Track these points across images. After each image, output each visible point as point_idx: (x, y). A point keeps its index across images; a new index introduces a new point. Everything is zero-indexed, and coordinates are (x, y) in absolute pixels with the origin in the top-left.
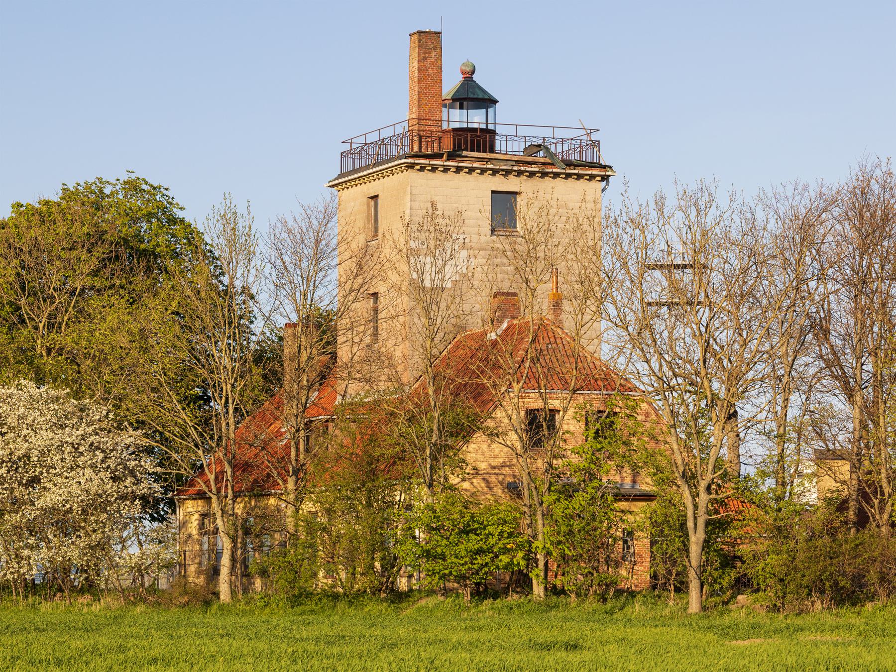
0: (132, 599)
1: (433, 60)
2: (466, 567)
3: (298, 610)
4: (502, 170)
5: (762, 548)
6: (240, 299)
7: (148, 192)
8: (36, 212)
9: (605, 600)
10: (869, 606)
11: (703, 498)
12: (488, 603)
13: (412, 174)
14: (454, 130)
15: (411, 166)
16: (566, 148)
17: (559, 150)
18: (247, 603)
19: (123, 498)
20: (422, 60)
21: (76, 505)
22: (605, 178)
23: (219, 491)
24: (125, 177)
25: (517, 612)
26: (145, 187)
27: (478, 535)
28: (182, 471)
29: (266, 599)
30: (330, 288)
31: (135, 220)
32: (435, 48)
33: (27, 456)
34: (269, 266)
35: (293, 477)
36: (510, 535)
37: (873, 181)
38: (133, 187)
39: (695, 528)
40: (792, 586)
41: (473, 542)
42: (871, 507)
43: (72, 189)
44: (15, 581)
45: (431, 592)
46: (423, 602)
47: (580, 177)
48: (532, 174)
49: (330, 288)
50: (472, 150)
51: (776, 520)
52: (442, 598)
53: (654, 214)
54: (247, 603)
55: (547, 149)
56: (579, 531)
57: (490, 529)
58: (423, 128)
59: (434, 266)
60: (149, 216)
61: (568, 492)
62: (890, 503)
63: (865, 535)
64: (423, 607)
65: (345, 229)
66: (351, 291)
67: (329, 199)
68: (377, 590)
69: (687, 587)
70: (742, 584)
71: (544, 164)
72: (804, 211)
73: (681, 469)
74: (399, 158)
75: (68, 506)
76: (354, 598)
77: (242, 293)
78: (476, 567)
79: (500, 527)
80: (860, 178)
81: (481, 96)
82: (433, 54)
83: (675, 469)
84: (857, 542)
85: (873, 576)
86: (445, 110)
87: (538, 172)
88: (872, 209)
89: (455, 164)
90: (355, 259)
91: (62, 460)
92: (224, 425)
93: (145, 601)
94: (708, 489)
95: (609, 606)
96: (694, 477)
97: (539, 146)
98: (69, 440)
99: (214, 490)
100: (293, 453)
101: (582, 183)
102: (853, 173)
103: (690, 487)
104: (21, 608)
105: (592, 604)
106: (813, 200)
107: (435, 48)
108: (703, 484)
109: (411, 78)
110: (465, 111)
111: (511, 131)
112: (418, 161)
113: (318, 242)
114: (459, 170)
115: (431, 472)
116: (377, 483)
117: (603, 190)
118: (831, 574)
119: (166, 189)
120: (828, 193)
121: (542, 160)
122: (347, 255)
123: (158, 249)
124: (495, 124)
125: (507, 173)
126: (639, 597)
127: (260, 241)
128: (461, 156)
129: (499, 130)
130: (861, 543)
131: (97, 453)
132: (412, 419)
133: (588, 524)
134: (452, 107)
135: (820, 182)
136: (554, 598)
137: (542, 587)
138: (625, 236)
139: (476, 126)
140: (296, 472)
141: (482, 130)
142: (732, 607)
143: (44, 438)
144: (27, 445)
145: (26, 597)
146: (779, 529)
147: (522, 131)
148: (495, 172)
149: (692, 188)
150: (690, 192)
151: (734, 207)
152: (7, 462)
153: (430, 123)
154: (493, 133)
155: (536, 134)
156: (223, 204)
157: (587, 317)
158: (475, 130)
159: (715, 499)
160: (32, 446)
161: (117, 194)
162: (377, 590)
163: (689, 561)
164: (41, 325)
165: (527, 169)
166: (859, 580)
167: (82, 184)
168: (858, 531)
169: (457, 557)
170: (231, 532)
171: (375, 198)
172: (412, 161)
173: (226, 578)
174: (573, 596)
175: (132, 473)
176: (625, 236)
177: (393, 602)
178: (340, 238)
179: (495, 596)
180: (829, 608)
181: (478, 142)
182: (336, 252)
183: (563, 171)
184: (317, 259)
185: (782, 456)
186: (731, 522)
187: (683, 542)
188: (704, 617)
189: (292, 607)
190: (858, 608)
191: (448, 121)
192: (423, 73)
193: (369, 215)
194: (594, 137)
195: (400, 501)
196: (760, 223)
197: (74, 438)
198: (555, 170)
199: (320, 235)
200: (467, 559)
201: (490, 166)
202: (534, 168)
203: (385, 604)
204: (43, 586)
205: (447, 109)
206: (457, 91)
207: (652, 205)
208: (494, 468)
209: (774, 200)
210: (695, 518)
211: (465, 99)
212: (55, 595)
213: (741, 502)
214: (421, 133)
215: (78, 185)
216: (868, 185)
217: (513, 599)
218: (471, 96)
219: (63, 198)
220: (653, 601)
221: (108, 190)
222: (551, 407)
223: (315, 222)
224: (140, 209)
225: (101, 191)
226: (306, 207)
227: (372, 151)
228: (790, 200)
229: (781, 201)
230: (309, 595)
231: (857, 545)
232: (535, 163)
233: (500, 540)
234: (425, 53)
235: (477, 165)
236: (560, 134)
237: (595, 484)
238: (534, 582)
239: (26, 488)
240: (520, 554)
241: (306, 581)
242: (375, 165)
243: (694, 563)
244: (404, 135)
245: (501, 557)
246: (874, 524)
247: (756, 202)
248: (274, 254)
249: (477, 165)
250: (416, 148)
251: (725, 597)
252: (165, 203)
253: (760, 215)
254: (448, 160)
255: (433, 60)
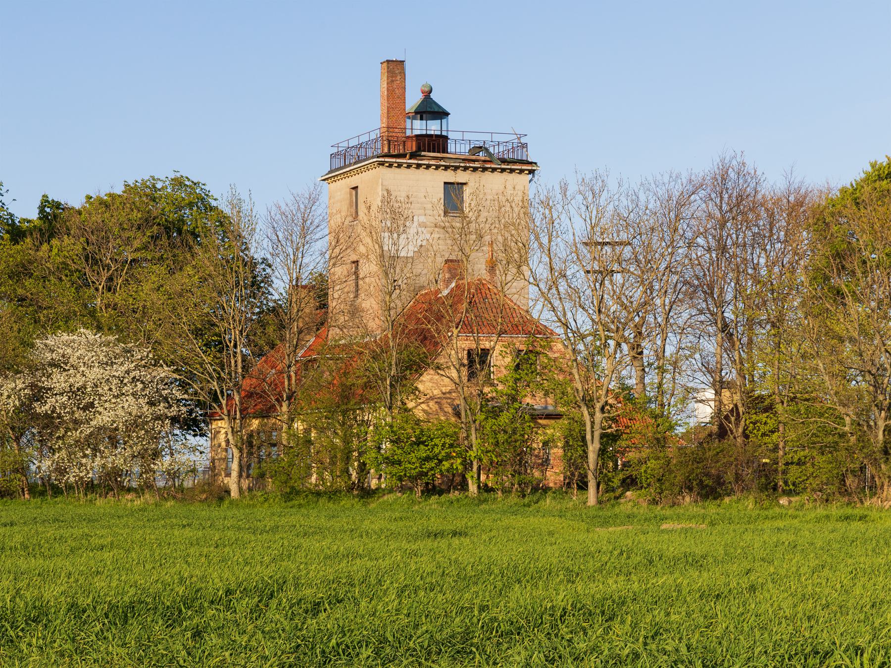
0: (166, 496)
1: (398, 82)
2: (417, 470)
3: (290, 504)
4: (452, 166)
5: (644, 455)
6: (260, 267)
7: (190, 187)
8: (102, 202)
9: (524, 496)
10: (727, 500)
11: (598, 416)
12: (434, 498)
13: (382, 170)
14: (417, 136)
15: (382, 164)
16: (501, 150)
17: (496, 151)
18: (251, 499)
19: (158, 418)
20: (390, 82)
21: (121, 424)
22: (531, 172)
23: (229, 411)
24: (172, 175)
25: (456, 506)
26: (187, 183)
27: (427, 446)
28: (201, 398)
29: (266, 496)
30: (314, 257)
31: (181, 208)
32: (400, 73)
33: (84, 387)
34: (267, 240)
35: (287, 402)
36: (451, 446)
37: (731, 170)
38: (178, 183)
39: (592, 440)
40: (667, 484)
41: (422, 452)
42: (729, 423)
43: (132, 185)
44: (76, 482)
45: (391, 491)
46: (386, 498)
47: (512, 171)
48: (475, 169)
49: (314, 257)
50: (429, 151)
51: (655, 433)
52: (399, 495)
53: (559, 197)
54: (251, 499)
55: (487, 150)
56: (503, 443)
57: (437, 441)
58: (391, 134)
59: (391, 240)
60: (191, 205)
61: (495, 413)
62: (743, 420)
63: (725, 443)
64: (384, 502)
65: (325, 211)
66: (331, 258)
67: (312, 189)
68: (350, 489)
69: (587, 486)
70: (630, 482)
71: (485, 161)
72: (678, 194)
73: (581, 394)
74: (373, 157)
75: (115, 425)
76: (333, 494)
77: (263, 262)
78: (424, 470)
79: (443, 440)
80: (721, 167)
81: (436, 110)
82: (399, 77)
83: (576, 394)
84: (718, 450)
85: (729, 477)
86: (409, 122)
87: (480, 168)
88: (730, 192)
89: (416, 162)
90: (333, 234)
91: (110, 389)
92: (233, 362)
93: (174, 498)
94: (602, 410)
95: (526, 500)
96: (591, 400)
97: (481, 147)
98: (117, 374)
99: (226, 412)
100: (286, 383)
101: (514, 176)
102: (715, 163)
103: (588, 407)
104: (81, 502)
105: (513, 499)
106: (684, 185)
107: (400, 73)
108: (598, 406)
109: (382, 96)
110: (425, 122)
111: (458, 136)
112: (387, 160)
113: (305, 221)
114: (418, 166)
115: (391, 399)
116: (349, 406)
117: (530, 181)
118: (697, 475)
119: (204, 185)
120: (697, 180)
121: (483, 158)
122: (326, 231)
123: (197, 230)
124: (448, 131)
125: (456, 168)
126: (549, 493)
127: (259, 221)
128: (420, 156)
129: (451, 135)
130: (722, 451)
131: (138, 383)
132: (375, 357)
133: (510, 437)
134: (414, 118)
135: (690, 171)
136: (485, 494)
137: (476, 485)
138: (538, 214)
139: (432, 133)
140: (289, 398)
141: (437, 136)
142: (622, 501)
143: (95, 373)
144: (84, 379)
145: (86, 495)
146: (658, 439)
147: (467, 136)
148: (447, 168)
149: (589, 177)
150: (587, 180)
151: (622, 190)
152: (69, 392)
153: (396, 130)
154: (446, 138)
155: (478, 139)
156: (230, 193)
157: (509, 278)
158: (431, 136)
159: (609, 417)
160: (87, 379)
161: (167, 188)
162: (350, 489)
163: (588, 466)
164: (101, 287)
165: (471, 165)
166: (719, 481)
167: (140, 181)
168: (719, 441)
169: (410, 463)
170: (239, 444)
171: (355, 188)
172: (383, 160)
173: (236, 480)
174: (500, 493)
175: (166, 399)
176: (538, 214)
177: (362, 497)
178: (321, 217)
179: (440, 493)
180: (696, 501)
181: (434, 145)
182: (319, 229)
183: (499, 166)
184: (304, 234)
185: (660, 385)
186: (622, 435)
187: (584, 451)
188: (600, 509)
189: (285, 502)
190: (718, 501)
191: (412, 129)
192: (391, 92)
193: (351, 202)
194: (523, 140)
195: (368, 420)
196: (642, 204)
197: (119, 372)
198: (493, 166)
199: (306, 215)
200: (418, 465)
201: (442, 163)
202: (477, 165)
203: (357, 500)
204: (99, 485)
205: (410, 120)
206: (419, 106)
207: (558, 190)
208: (444, 394)
209: (654, 186)
210: (592, 432)
211: (424, 112)
212: (107, 493)
213: (630, 420)
214: (390, 138)
215: (136, 182)
216: (727, 173)
217: (454, 495)
218: (429, 110)
219: (124, 192)
220: (561, 497)
221: (159, 185)
222: (482, 347)
223: (302, 206)
224: (183, 199)
225: (154, 187)
226: (295, 195)
227: (354, 152)
228: (667, 186)
229: (660, 187)
230: (298, 493)
231: (718, 453)
232: (477, 161)
233: (443, 449)
234: (392, 77)
235: (432, 162)
236: (497, 138)
237: (516, 405)
238: (470, 482)
239: (84, 411)
240: (459, 461)
241: (295, 482)
242: (355, 163)
243: (592, 467)
244: (376, 140)
245: (444, 463)
246: (732, 437)
247: (639, 187)
248: (270, 231)
249: (432, 162)
250: (386, 150)
251: (617, 494)
252: (203, 195)
253: (642, 198)
254: (410, 159)
255: (398, 82)
